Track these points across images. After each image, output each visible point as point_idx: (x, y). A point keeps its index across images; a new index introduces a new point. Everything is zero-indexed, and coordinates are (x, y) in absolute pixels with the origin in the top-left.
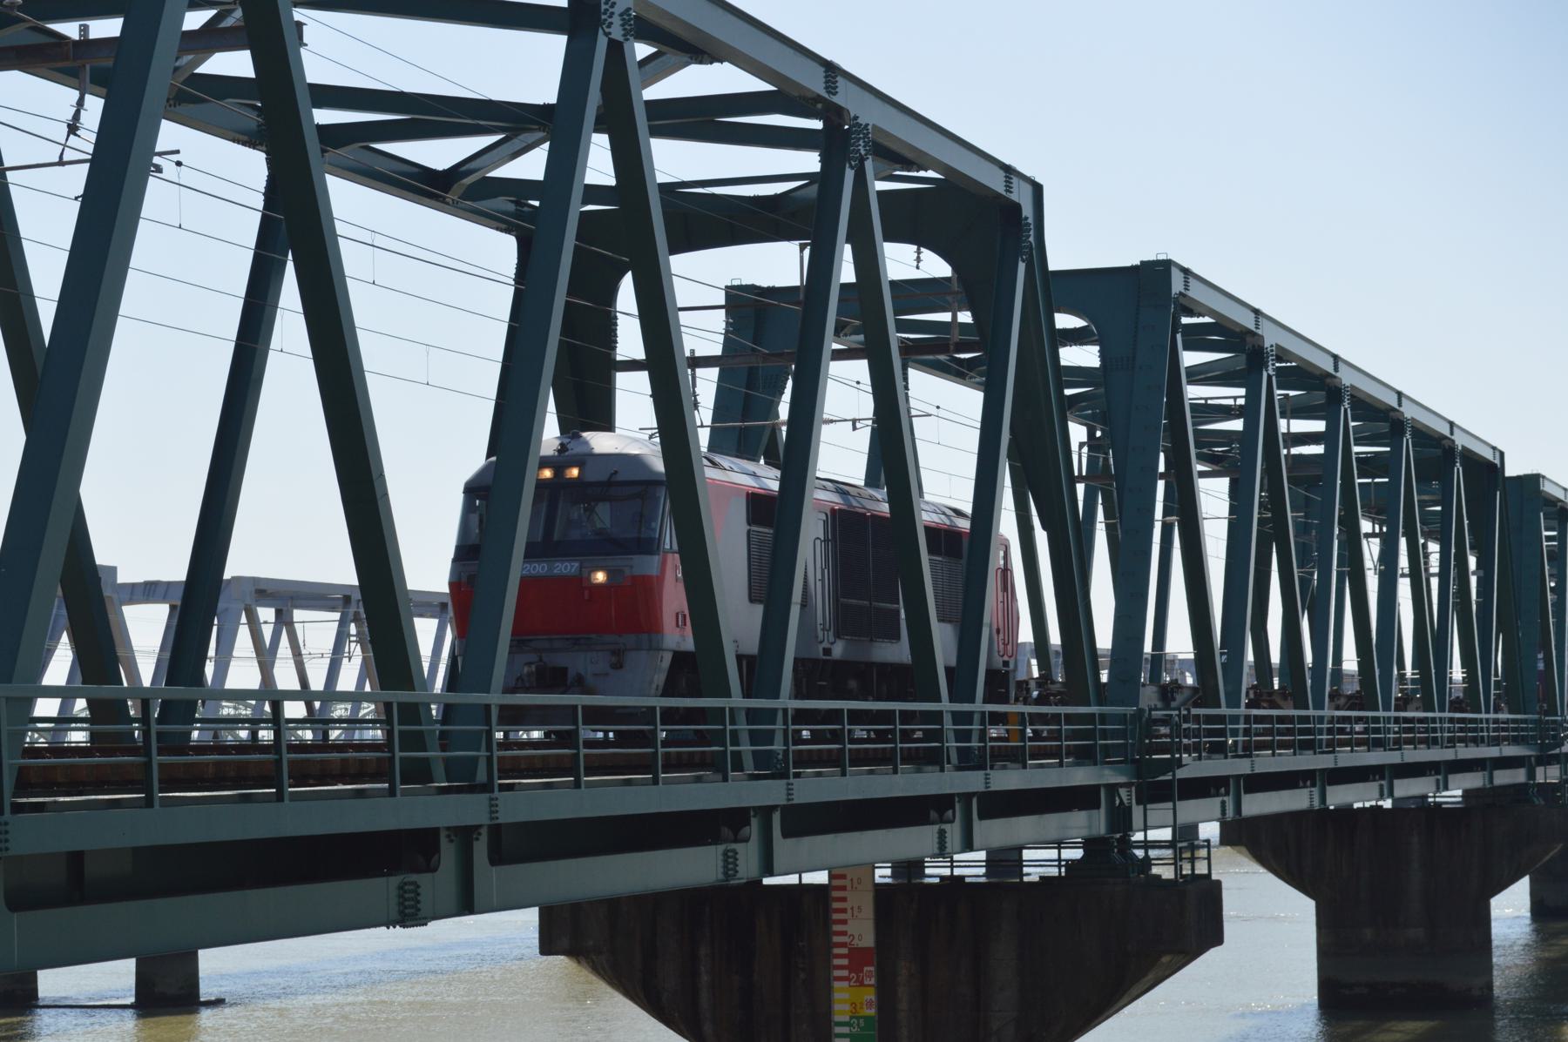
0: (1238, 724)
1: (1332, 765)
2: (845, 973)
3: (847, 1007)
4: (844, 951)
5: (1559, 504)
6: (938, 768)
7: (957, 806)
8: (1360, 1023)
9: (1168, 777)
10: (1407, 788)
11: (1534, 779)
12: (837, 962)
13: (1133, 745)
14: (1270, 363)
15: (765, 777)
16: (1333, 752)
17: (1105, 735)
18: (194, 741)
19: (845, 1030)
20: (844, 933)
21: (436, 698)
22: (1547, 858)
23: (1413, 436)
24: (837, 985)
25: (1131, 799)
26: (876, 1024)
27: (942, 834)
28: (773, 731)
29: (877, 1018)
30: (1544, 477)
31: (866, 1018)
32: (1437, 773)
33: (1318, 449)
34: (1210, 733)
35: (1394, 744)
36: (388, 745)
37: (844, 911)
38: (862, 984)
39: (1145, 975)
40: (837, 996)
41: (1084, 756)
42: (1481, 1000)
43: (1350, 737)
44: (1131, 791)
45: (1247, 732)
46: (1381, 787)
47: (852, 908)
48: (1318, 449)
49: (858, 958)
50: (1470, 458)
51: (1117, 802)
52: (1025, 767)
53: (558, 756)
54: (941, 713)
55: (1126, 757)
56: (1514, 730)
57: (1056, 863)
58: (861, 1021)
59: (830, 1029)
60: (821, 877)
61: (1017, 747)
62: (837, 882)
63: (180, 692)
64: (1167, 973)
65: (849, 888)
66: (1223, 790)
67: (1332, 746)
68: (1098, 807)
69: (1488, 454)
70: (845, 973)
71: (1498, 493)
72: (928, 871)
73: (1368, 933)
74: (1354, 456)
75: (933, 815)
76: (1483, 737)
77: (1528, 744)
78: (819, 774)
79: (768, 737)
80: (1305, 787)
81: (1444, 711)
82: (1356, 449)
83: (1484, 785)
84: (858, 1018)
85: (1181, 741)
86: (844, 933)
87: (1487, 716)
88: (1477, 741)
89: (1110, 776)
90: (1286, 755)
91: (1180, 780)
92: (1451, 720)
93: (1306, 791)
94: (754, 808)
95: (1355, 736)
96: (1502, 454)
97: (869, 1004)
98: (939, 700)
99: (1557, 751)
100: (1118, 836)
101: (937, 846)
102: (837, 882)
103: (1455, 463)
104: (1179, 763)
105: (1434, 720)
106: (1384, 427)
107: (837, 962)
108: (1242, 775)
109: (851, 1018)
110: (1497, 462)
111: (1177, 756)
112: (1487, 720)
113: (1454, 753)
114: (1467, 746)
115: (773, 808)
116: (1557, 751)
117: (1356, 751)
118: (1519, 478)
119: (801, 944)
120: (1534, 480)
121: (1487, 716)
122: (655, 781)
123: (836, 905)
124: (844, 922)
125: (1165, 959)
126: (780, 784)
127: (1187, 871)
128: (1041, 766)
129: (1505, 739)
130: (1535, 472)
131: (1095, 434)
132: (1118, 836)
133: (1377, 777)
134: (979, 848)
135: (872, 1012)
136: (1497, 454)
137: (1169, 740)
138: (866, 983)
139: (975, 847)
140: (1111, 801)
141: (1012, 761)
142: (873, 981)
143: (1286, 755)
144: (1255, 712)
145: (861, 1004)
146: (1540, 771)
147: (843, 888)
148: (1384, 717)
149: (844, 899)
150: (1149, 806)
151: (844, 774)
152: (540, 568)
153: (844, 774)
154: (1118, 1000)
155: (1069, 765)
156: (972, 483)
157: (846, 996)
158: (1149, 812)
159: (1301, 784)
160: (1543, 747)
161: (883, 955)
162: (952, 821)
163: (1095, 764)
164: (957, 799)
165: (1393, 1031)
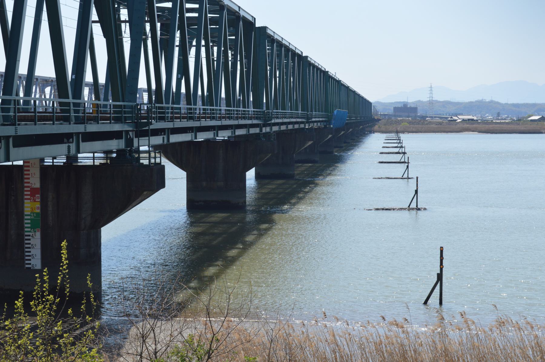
0: (169, 110)
1: (199, 125)
2: (29, 197)
3: (29, 209)
4: (29, 189)
5: (272, 37)
6: (68, 123)
7: (74, 137)
8: (203, 214)
9: (147, 128)
11: (262, 132)
12: (26, 193)
13: (134, 116)
15: (7, 125)
16: (200, 121)
19: (29, 217)
20: (29, 183)
22: (266, 159)
24: (26, 201)
25: (133, 136)
26: (40, 215)
27: (69, 147)
28: (10, 108)
29: (40, 213)
30: (268, 28)
31: (37, 213)
32: (232, 129)
33: (196, 15)
34: (160, 113)
37: (29, 175)
38: (35, 201)
40: (26, 205)
41: (118, 120)
42: (241, 207)
43: (186, 115)
44: (133, 133)
45: (172, 113)
46: (214, 133)
47: (32, 174)
48: (196, 15)
49: (33, 192)
50: (245, 20)
51: (129, 137)
52: (98, 123)
54: (70, 103)
55: (132, 121)
56: (290, 115)
57: (92, 158)
58: (35, 214)
59: (23, 217)
60: (21, 163)
61: (95, 116)
62: (26, 164)
65: (31, 166)
67: (172, 119)
68: (122, 139)
69: (250, 19)
70: (29, 197)
72: (46, 160)
73: (204, 184)
74: (208, 18)
75: (65, 140)
76: (232, 116)
77: (261, 119)
78: (26, 124)
79: (8, 110)
80: (189, 133)
81: (217, 107)
82: (209, 15)
84: (33, 213)
85: (152, 115)
86: (29, 183)
87: (234, 109)
89: (126, 128)
90: (184, 121)
93: (190, 134)
94: (3, 137)
96: (255, 19)
97: (38, 208)
98: (69, 98)
100: (129, 149)
101: (67, 151)
102: (26, 164)
104: (151, 123)
106: (217, 8)
107: (26, 193)
108: (81, 132)
109: (31, 213)
110: (253, 21)
111: (150, 121)
113: (175, 125)
114: (241, 120)
115: (9, 137)
117: (207, 121)
118: (259, 27)
119: (12, 186)
120: (264, 29)
121: (234, 109)
122: (53, 124)
123: (25, 172)
124: (29, 179)
125: (145, 193)
127: (153, 161)
128: (103, 123)
129: (240, 118)
130: (265, 26)
131: (115, 6)
132: (129, 149)
133: (191, 131)
134: (88, 152)
135: (39, 211)
136: (253, 19)
138: (37, 200)
139: (80, 152)
140: (126, 136)
141: (65, 121)
142: (39, 200)
143: (184, 121)
144: (175, 106)
145: (35, 208)
147: (28, 166)
148: (194, 108)
149: (29, 170)
150: (140, 138)
151: (35, 124)
153: (35, 124)
154: (127, 208)
155: (113, 123)
157: (29, 205)
159: (188, 132)
160: (265, 121)
161: (43, 191)
162: (73, 142)
163: (122, 123)
164: (74, 135)
165: (214, 217)
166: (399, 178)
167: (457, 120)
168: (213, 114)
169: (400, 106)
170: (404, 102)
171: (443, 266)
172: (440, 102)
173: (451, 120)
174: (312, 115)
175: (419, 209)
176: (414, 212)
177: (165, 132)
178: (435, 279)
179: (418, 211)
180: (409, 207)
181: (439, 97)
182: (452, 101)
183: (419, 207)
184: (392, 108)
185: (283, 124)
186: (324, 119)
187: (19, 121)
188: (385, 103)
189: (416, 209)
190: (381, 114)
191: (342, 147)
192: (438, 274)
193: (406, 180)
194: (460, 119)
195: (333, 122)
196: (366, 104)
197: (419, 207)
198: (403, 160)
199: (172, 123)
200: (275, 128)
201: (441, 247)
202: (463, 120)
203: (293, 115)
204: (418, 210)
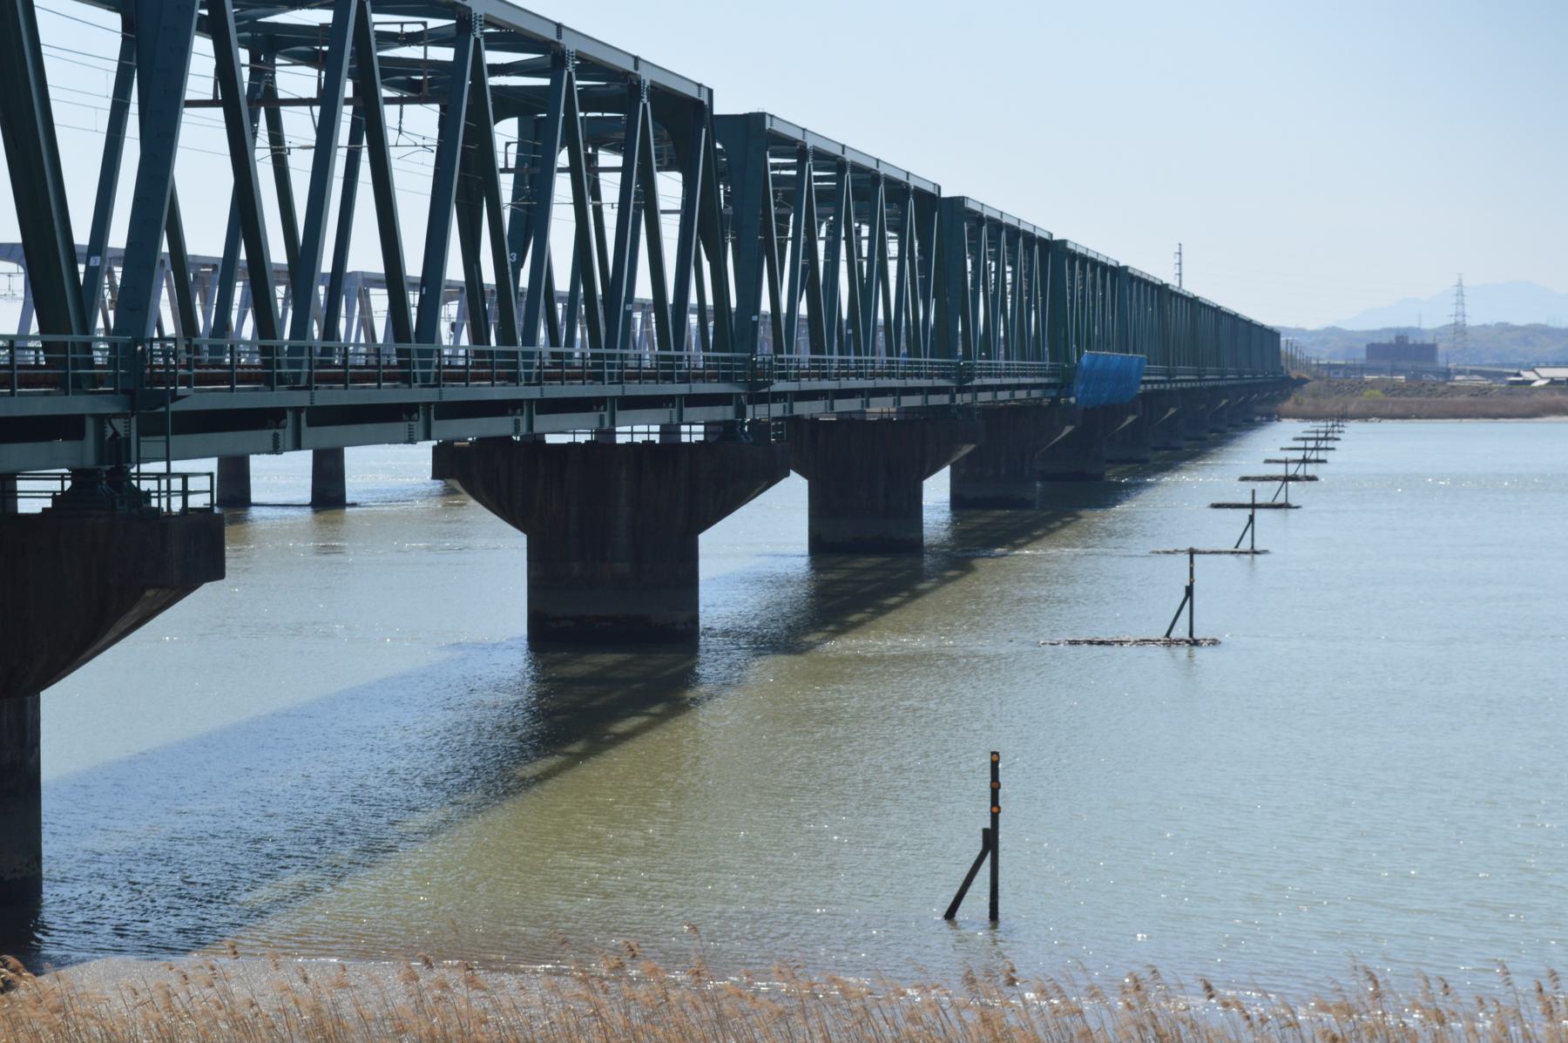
7: (525, 407)
10: (842, 405)
14: (478, 27)
17: (737, 368)
18: (645, 368)
21: (286, 343)
23: (885, 184)
27: (410, 428)
32: (894, 395)
33: (794, 173)
35: (618, 378)
36: (465, 367)
39: (130, 609)
44: (130, 422)
48: (794, 173)
53: (26, 374)
63: (328, 344)
64: (155, 607)
66: (519, 411)
69: (930, 189)
71: (704, 130)
75: (404, 416)
83: (671, 421)
87: (866, 358)
88: (918, 376)
89: (106, 407)
91: (175, 414)
92: (931, 363)
95: (544, 371)
99: (970, 384)
100: (108, 467)
103: (640, 98)
105: (824, 361)
110: (936, 193)
112: (925, 363)
116: (970, 384)
120: (1064, 242)
121: (866, 358)
126: (687, 385)
130: (761, 111)
137: (163, 371)
140: (100, 432)
141: (404, 382)
146: (958, 396)
152: (1131, 349)
156: (309, 175)
158: (142, 444)
160: (961, 381)
166: (1225, 552)
167: (1534, 381)
168: (861, 368)
169: (1385, 340)
170: (1398, 330)
171: (999, 808)
172: (1516, 328)
173: (1517, 383)
174: (971, 366)
175: (1196, 643)
176: (1183, 651)
177: (522, 408)
178: (978, 847)
179: (1196, 649)
180: (1168, 635)
181: (1476, 318)
182: (1551, 324)
183: (1196, 636)
184: (1364, 346)
185: (1019, 387)
186: (1052, 380)
187: (445, 380)
188: (1353, 332)
189: (1188, 642)
190: (1318, 365)
191: (1179, 448)
192: (985, 831)
193: (1248, 557)
194: (1542, 378)
195: (1079, 387)
196: (1265, 338)
197: (1196, 636)
198: (1281, 500)
199: (538, 388)
200: (985, 397)
201: (993, 753)
202: (1553, 382)
203: (991, 369)
204: (1192, 645)
